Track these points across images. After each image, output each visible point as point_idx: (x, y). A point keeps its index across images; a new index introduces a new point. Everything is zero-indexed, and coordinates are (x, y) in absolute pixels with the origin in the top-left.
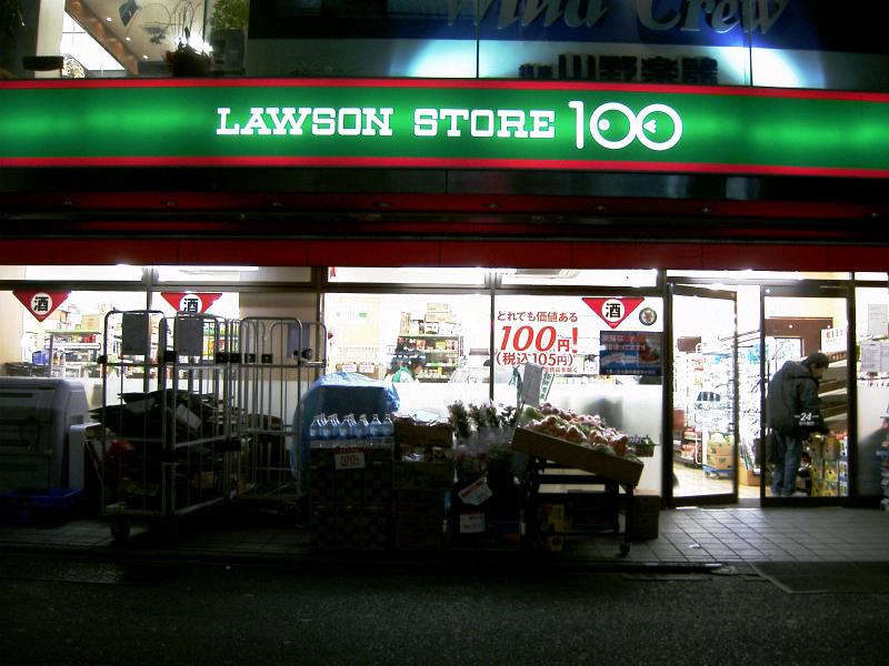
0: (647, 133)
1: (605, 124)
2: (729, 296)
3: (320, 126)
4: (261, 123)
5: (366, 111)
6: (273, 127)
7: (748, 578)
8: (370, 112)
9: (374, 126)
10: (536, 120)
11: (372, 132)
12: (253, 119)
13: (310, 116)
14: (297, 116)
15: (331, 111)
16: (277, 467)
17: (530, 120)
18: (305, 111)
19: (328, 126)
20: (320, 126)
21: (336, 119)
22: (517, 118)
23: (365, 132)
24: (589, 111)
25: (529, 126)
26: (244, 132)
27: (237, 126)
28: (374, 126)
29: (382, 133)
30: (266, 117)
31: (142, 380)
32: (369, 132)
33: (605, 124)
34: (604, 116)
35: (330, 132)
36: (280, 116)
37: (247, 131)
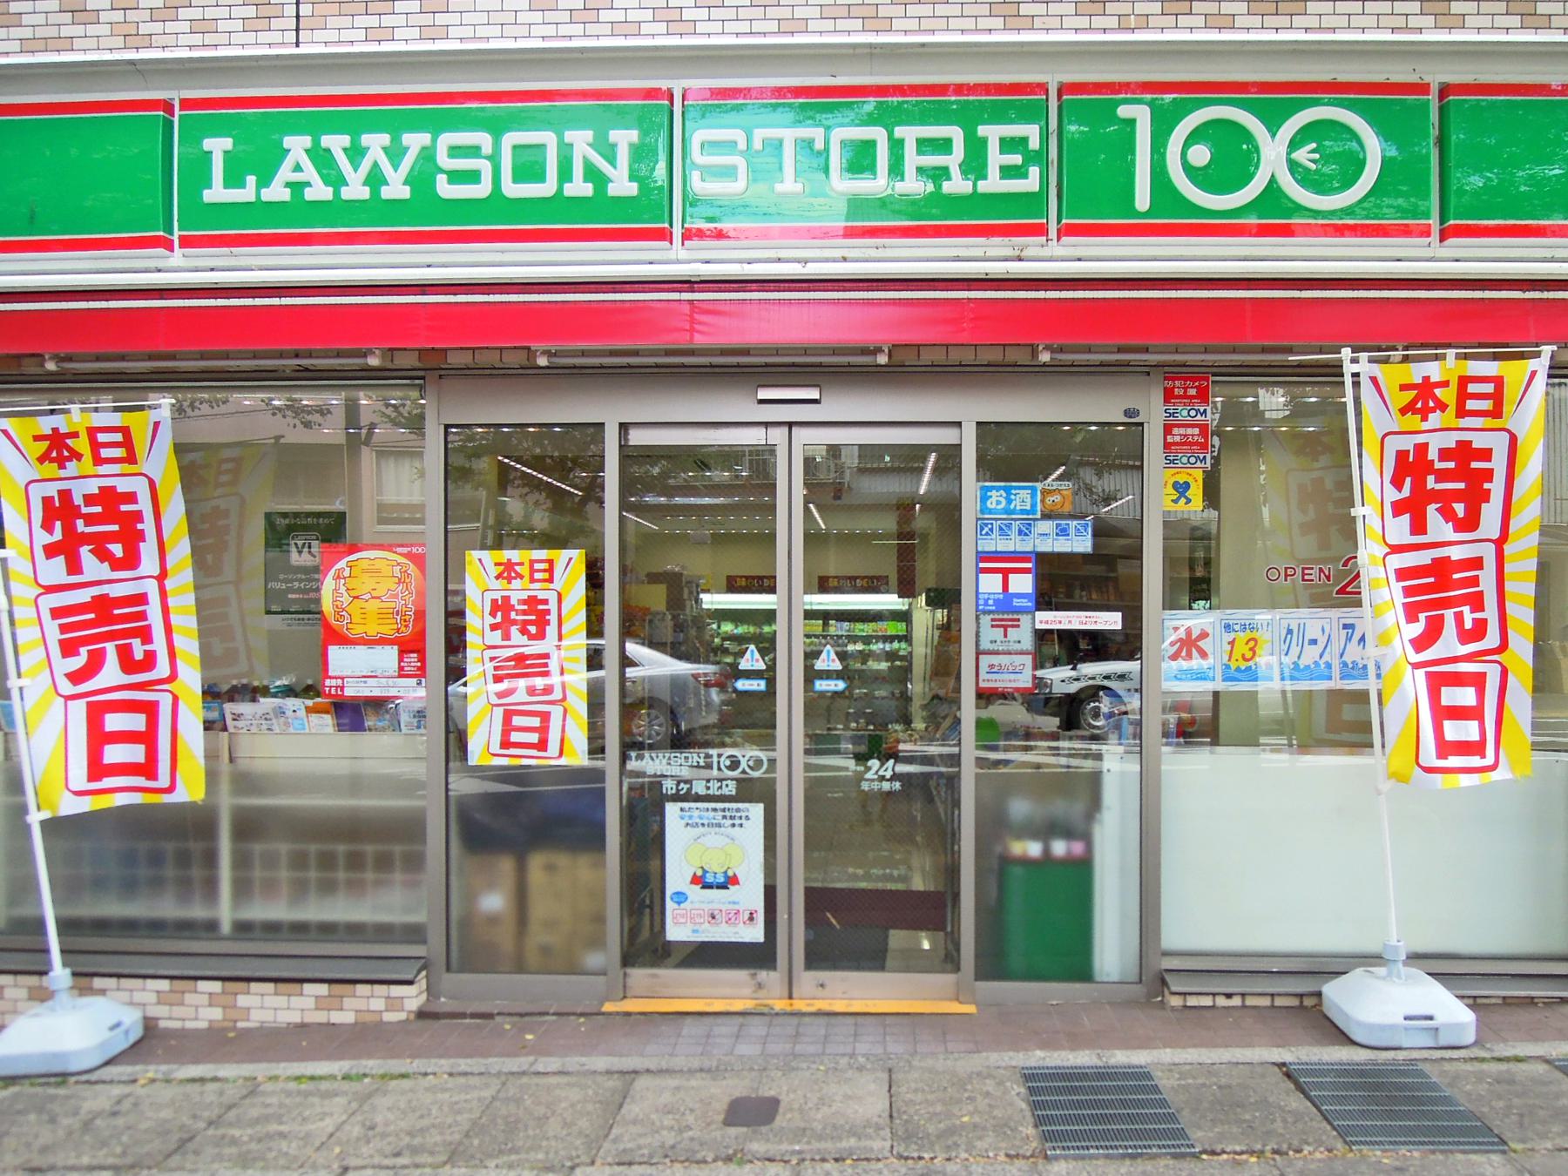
0: (1293, 166)
1: (1200, 155)
2: (21, 689)
3: (456, 177)
4: (310, 173)
5: (569, 136)
6: (338, 181)
7: (292, 1085)
8: (581, 140)
9: (592, 173)
10: (993, 147)
11: (587, 190)
12: (288, 163)
13: (427, 154)
14: (395, 153)
15: (484, 140)
16: (40, 925)
17: (976, 149)
18: (415, 141)
19: (473, 177)
20: (456, 177)
21: (494, 158)
22: (944, 145)
23: (570, 190)
24: (1162, 126)
25: (975, 164)
26: (268, 195)
27: (251, 180)
28: (592, 173)
29: (613, 190)
30: (322, 158)
31: (1011, 576)
32: (579, 187)
33: (1200, 155)
34: (1194, 137)
35: (482, 190)
36: (356, 153)
37: (277, 192)
